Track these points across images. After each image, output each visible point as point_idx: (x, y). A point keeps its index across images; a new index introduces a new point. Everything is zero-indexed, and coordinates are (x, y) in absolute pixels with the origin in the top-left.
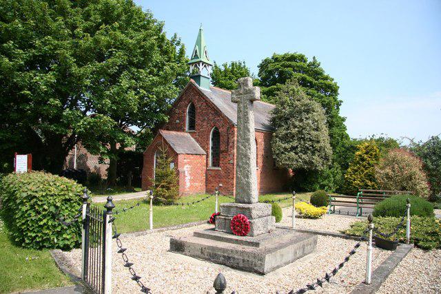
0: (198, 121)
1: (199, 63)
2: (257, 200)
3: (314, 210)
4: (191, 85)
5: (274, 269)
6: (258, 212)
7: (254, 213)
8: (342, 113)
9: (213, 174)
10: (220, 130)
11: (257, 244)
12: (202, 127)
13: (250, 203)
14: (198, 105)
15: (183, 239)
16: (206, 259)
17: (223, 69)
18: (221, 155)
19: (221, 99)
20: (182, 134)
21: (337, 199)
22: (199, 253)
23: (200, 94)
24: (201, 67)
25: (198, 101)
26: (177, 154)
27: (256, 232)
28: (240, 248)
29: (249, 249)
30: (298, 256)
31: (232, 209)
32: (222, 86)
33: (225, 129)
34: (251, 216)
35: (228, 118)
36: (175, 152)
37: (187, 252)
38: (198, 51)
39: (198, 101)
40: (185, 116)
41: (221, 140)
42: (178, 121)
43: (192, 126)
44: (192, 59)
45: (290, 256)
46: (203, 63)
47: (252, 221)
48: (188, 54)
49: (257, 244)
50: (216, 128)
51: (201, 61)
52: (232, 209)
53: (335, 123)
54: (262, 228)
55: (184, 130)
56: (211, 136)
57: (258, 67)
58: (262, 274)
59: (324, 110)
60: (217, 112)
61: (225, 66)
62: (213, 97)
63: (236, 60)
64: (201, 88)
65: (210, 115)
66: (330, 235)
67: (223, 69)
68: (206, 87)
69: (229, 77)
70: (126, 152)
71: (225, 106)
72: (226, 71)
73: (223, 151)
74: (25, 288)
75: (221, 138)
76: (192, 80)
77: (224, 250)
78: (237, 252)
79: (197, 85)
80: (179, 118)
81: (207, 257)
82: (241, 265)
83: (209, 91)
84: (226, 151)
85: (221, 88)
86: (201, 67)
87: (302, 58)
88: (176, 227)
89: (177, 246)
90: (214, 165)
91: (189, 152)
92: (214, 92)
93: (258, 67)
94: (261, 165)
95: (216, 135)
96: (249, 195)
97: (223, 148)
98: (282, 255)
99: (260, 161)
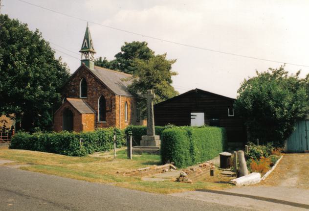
1: (88, 52)
12: (92, 95)
18: (107, 114)
23: (90, 73)
36: (79, 112)
39: (89, 78)
42: (73, 91)
50: (102, 96)
51: (90, 51)
57: (126, 43)
59: (273, 92)
63: (7, 14)
65: (98, 88)
73: (108, 111)
74: (150, 169)
79: (87, 67)
80: (74, 89)
84: (111, 111)
90: (101, 120)
93: (126, 43)
94: (129, 119)
95: (103, 101)
97: (108, 109)
99: (129, 116)
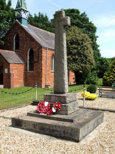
0: (21, 44)
2: (68, 91)
3: (88, 94)
4: (16, 23)
5: (84, 137)
6: (69, 99)
7: (68, 99)
8: (98, 42)
9: (30, 75)
10: (34, 50)
11: (71, 121)
13: (65, 93)
14: (20, 35)
15: (20, 118)
16: (36, 132)
17: (33, 16)
18: (34, 64)
19: (33, 31)
20: (12, 52)
21: (103, 89)
22: (32, 127)
24: (22, 12)
25: (21, 33)
26: (9, 64)
27: (69, 112)
28: (61, 123)
29: (67, 124)
30: (95, 126)
31: (52, 97)
32: (32, 24)
33: (37, 49)
34: (66, 103)
35: (38, 43)
36: (8, 62)
37: (23, 126)
38: (20, 2)
39: (21, 33)
40: (13, 42)
41: (33, 57)
42: (9, 44)
43: (17, 47)
44: (17, 8)
45: (91, 127)
46: (23, 10)
47: (67, 105)
48: (14, 6)
49: (71, 121)
50: (31, 48)
51: (22, 9)
52: (52, 97)
53: (95, 47)
54: (72, 109)
55: (13, 50)
56: (28, 53)
58: (78, 141)
60: (32, 39)
61: (35, 14)
62: (29, 30)
64: (22, 25)
66: (107, 111)
67: (33, 16)
68: (25, 25)
69: (39, 21)
70: (62, 34)
71: (37, 36)
72: (36, 17)
75: (34, 54)
76: (17, 20)
77: (50, 125)
78: (59, 126)
80: (9, 43)
81: (38, 130)
82: (63, 135)
83: (27, 27)
84: (38, 62)
85: (32, 25)
86: (22, 12)
87: (78, 12)
88: (12, 108)
89: (17, 123)
90: (30, 69)
91: (16, 63)
92: (30, 28)
95: (32, 53)
96: (63, 88)
97: (35, 60)
98: (88, 127)
